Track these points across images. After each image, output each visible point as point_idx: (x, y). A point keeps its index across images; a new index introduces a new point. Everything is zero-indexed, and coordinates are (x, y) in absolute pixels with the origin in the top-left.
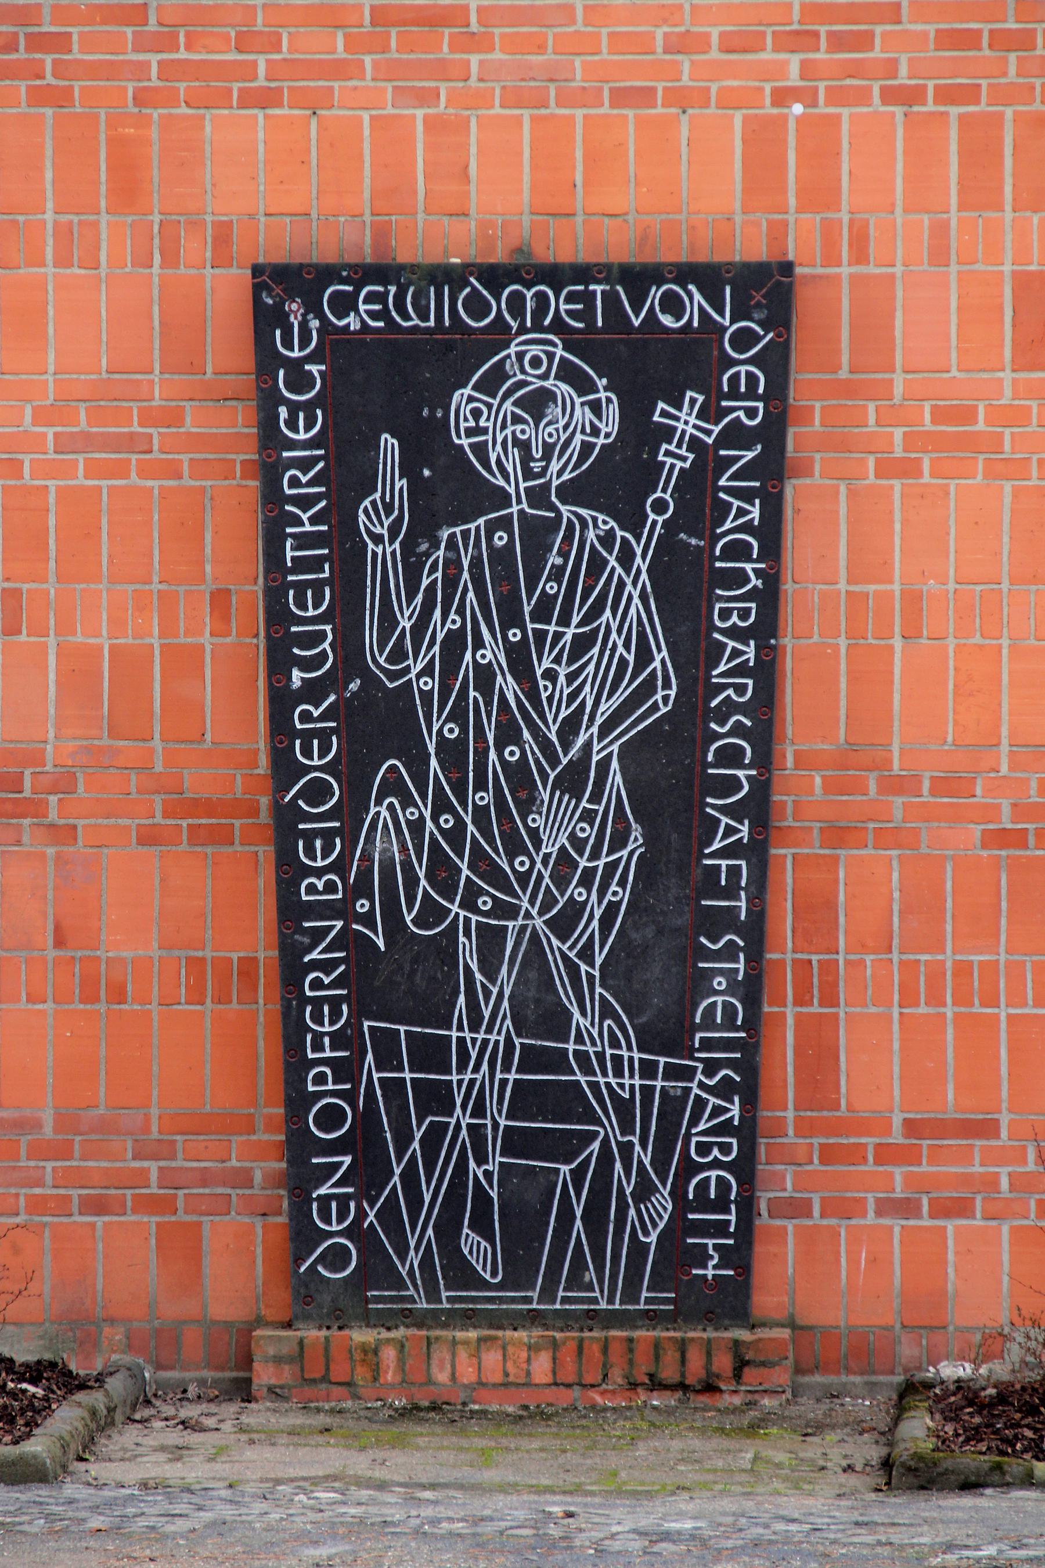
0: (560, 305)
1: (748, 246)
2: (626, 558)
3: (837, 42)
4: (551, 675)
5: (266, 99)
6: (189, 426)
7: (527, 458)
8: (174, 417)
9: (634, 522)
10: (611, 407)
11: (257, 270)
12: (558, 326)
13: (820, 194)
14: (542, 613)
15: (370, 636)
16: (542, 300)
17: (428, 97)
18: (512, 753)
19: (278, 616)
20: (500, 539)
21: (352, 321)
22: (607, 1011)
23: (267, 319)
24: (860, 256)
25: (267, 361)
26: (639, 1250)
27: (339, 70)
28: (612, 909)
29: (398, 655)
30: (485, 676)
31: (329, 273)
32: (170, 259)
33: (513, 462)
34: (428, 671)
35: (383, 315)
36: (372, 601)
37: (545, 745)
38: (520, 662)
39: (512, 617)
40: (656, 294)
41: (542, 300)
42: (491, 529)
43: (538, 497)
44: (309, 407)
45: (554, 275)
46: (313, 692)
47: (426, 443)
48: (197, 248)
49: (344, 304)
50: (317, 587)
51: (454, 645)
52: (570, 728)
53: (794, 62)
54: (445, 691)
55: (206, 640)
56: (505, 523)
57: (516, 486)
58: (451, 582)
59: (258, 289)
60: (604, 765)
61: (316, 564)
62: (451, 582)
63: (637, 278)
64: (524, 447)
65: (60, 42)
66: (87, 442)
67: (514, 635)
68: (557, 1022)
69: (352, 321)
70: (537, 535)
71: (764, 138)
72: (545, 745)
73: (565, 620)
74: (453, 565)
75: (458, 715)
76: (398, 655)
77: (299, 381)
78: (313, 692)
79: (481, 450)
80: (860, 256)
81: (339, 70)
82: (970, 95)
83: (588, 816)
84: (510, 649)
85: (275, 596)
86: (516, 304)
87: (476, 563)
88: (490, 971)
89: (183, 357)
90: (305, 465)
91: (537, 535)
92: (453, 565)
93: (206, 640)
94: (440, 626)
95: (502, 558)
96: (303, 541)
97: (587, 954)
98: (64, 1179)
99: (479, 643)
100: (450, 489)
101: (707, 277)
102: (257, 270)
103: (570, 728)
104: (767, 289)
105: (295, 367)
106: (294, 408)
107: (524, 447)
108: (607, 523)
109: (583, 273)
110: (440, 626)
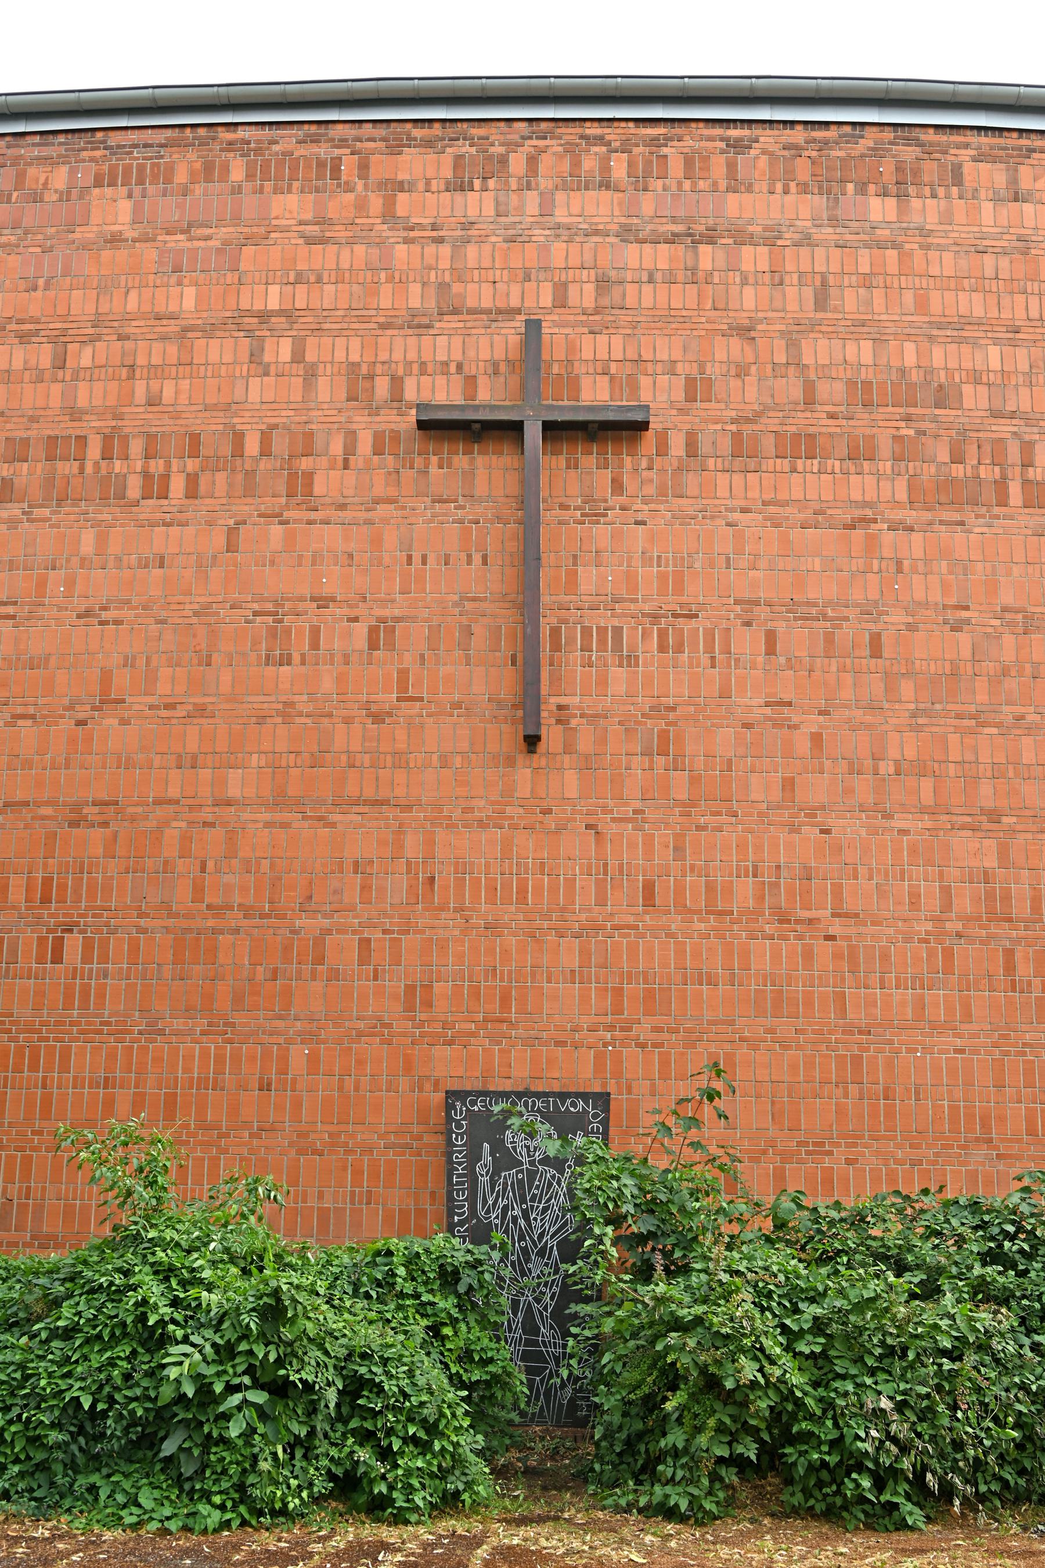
0: (539, 1104)
1: (597, 1089)
2: (559, 1183)
3: (622, 1029)
4: (535, 1219)
5: (450, 1043)
6: (425, 1141)
7: (529, 1151)
8: (419, 1138)
9: (562, 1173)
10: (335, 412)
11: (447, 1092)
12: (539, 1111)
13: (617, 1074)
14: (533, 1200)
15: (479, 1206)
16: (534, 1102)
17: (499, 1043)
18: (523, 1244)
19: (450, 1199)
20: (520, 1176)
21: (476, 1108)
22: (552, 1327)
23: (449, 1107)
24: (629, 1092)
25: (449, 1119)
26: (561, 1405)
27: (473, 1034)
28: (554, 1294)
29: (488, 1212)
30: (515, 1219)
31: (469, 1093)
32: (421, 1090)
33: (524, 1152)
34: (497, 1217)
35: (485, 1106)
36: (480, 1195)
37: (533, 1241)
38: (526, 1215)
39: (523, 1201)
40: (569, 1101)
41: (534, 1102)
42: (517, 1172)
43: (532, 1163)
44: (462, 1134)
45: (538, 1095)
46: (461, 1223)
47: (498, 1146)
48: (428, 1086)
49: (473, 1103)
50: (463, 1190)
51: (505, 1209)
52: (541, 1236)
53: (609, 1035)
54: (502, 1224)
55: (428, 1207)
56: (522, 1171)
57: (525, 1160)
58: (505, 1189)
59: (447, 1098)
60: (552, 1248)
61: (463, 1183)
62: (505, 1189)
63: (563, 1096)
64: (528, 1147)
65: (389, 1026)
66: (393, 1146)
67: (524, 1206)
68: (536, 1331)
69: (476, 1108)
70: (532, 1175)
71: (599, 1058)
72: (533, 1241)
73: (540, 1202)
74: (505, 1184)
75: (506, 1232)
76: (488, 1212)
77: (459, 1126)
78: (461, 1223)
79: (515, 1148)
80: (629, 1092)
81: (473, 1034)
82: (662, 1045)
83: (546, 1264)
84: (523, 1210)
85: (450, 1193)
86: (526, 1104)
87: (513, 1183)
88: (515, 1314)
89: (423, 1121)
90: (460, 1152)
91: (532, 1175)
92: (505, 1184)
93: (428, 1207)
94: (501, 1203)
95: (521, 1182)
96: (459, 1176)
97: (546, 1309)
98: (70, 1032)
99: (513, 1209)
100: (505, 1160)
101: (585, 1096)
102: (447, 1092)
103: (541, 1236)
104: (603, 1100)
105: (458, 1122)
106: (457, 1134)
107: (528, 1147)
108: (553, 1172)
109: (546, 1095)
110: (501, 1203)
